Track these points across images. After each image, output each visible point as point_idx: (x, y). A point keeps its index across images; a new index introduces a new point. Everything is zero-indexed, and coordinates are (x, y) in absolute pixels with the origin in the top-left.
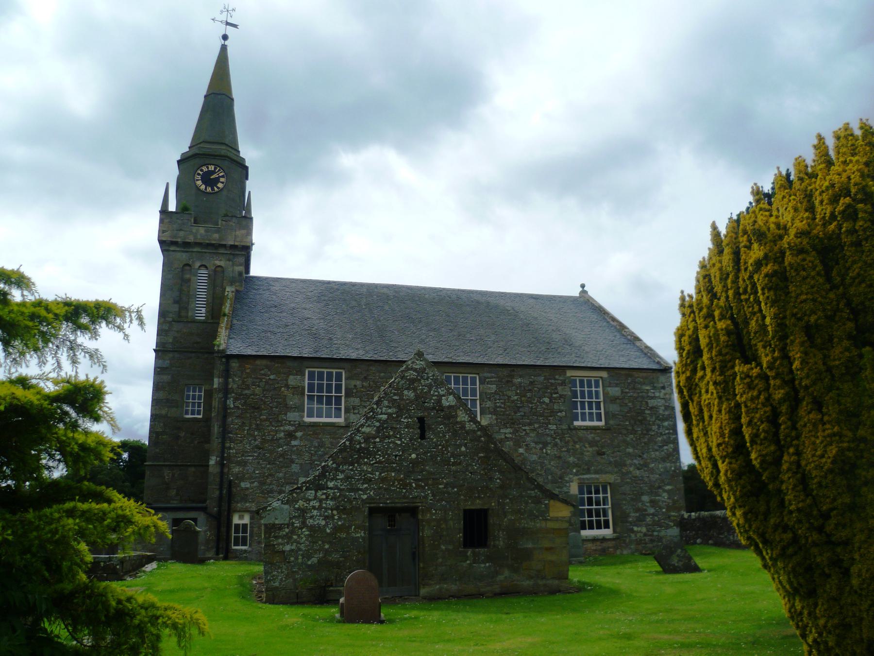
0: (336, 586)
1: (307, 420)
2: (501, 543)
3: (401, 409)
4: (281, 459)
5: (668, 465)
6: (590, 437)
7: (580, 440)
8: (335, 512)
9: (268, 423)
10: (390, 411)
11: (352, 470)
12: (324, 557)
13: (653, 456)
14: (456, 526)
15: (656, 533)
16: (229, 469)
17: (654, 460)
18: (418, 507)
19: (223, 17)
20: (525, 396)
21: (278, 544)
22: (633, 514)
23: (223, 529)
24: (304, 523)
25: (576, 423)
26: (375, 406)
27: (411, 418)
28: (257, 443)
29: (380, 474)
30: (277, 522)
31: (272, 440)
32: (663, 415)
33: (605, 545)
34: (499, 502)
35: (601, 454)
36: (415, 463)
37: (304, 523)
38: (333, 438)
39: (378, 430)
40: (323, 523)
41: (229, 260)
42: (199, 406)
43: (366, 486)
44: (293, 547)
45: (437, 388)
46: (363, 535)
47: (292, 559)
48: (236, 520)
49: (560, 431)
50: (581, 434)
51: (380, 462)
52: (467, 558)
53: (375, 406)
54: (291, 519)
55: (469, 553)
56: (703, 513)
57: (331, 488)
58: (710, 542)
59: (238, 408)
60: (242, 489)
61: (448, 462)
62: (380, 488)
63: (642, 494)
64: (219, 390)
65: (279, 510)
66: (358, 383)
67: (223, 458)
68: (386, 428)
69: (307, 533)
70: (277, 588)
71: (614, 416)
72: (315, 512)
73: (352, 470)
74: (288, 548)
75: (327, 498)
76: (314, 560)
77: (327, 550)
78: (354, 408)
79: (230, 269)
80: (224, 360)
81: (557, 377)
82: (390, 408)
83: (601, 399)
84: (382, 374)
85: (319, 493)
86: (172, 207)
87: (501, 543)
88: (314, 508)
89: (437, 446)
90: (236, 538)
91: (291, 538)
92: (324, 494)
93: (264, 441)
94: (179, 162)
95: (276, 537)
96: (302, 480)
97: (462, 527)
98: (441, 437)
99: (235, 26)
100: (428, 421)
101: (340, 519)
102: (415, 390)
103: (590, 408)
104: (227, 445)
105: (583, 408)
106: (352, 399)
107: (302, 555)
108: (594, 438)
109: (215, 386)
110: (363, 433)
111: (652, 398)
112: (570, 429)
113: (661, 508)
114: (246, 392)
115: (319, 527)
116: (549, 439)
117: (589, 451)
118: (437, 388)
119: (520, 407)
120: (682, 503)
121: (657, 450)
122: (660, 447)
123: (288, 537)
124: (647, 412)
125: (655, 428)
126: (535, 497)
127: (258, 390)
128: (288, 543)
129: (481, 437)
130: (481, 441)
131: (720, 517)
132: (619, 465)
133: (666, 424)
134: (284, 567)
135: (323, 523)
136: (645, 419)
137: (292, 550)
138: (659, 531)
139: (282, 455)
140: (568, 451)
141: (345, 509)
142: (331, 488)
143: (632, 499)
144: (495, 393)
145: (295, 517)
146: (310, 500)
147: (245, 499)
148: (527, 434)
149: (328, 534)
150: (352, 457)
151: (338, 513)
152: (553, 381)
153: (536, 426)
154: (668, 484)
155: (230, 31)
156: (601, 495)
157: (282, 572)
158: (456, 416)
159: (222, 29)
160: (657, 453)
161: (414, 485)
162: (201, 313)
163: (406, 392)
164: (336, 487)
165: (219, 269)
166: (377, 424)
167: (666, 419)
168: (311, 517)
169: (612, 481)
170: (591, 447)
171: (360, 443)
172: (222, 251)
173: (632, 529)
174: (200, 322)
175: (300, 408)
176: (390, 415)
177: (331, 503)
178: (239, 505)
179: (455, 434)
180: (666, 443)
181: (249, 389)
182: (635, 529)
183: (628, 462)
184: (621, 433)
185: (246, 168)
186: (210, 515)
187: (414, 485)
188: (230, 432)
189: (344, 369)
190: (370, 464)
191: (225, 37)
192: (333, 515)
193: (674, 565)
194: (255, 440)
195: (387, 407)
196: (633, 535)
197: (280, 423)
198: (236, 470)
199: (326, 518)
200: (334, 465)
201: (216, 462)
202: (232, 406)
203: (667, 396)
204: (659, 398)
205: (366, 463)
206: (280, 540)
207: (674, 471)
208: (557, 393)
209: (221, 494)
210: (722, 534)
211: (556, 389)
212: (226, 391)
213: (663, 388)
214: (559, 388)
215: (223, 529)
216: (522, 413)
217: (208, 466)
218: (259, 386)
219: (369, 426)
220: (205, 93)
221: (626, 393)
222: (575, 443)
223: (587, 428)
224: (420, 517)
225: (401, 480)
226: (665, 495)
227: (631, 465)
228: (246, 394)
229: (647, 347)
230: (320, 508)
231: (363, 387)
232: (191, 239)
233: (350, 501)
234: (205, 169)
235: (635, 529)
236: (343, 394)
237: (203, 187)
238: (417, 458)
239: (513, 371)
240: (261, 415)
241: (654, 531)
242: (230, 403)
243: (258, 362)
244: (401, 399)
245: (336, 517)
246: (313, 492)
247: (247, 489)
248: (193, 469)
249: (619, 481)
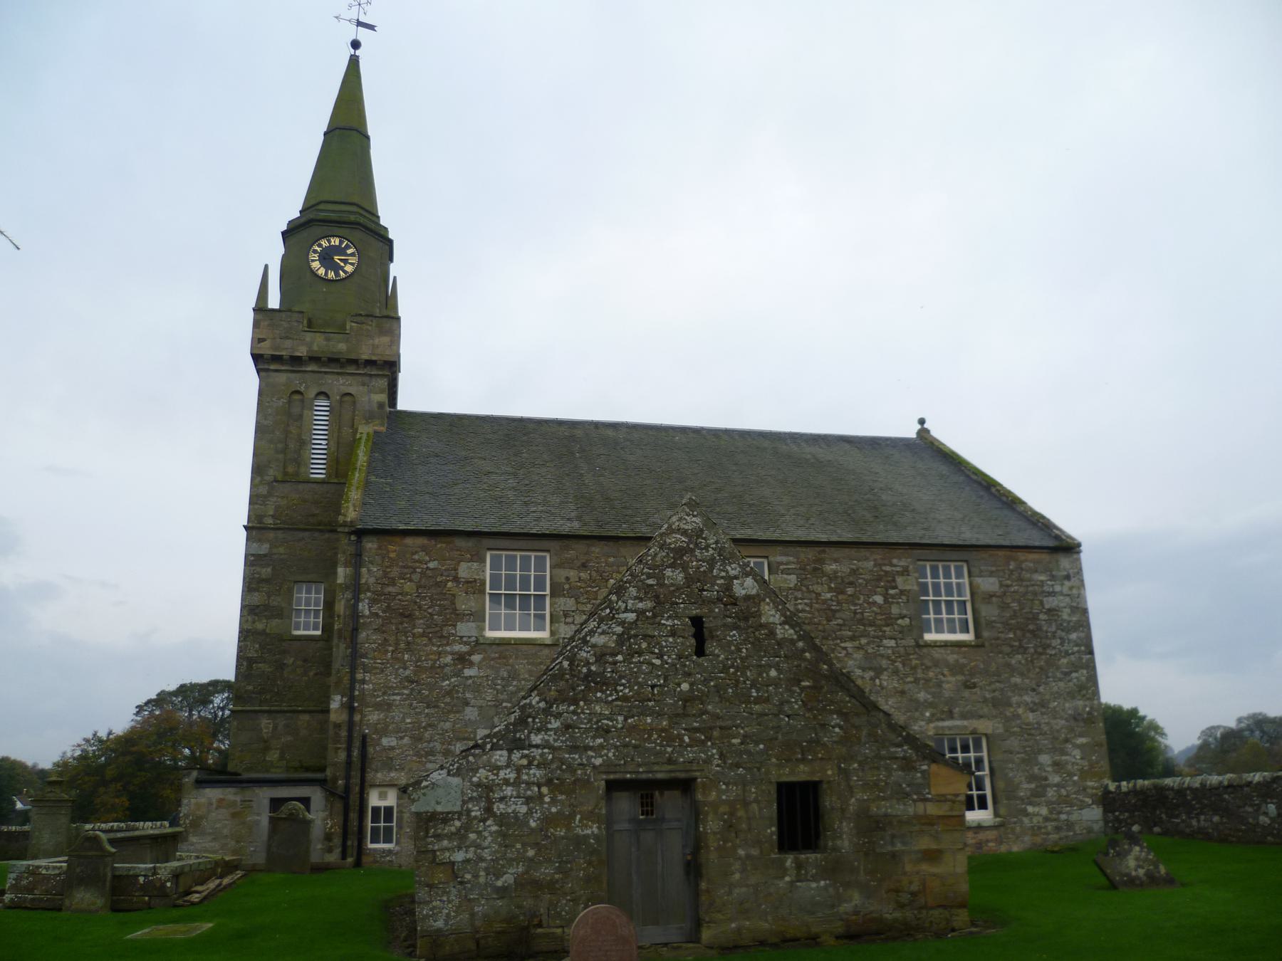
0: (549, 927)
1: (490, 634)
2: (845, 844)
3: (661, 600)
4: (448, 700)
5: (1081, 703)
6: (952, 658)
7: (936, 664)
8: (545, 790)
9: (425, 641)
10: (640, 605)
11: (574, 712)
12: (527, 872)
13: (1055, 689)
14: (763, 818)
15: (1063, 817)
16: (363, 716)
17: (1057, 696)
18: (695, 779)
19: (353, 14)
20: (843, 593)
21: (443, 850)
22: (1026, 786)
23: (353, 816)
24: (489, 810)
25: (928, 637)
26: (614, 598)
27: (677, 617)
28: (407, 672)
29: (626, 719)
30: (439, 809)
31: (432, 667)
32: (1069, 622)
33: (982, 836)
34: (839, 767)
35: (969, 686)
36: (688, 699)
37: (489, 810)
38: (532, 664)
39: (621, 639)
40: (524, 809)
41: (363, 385)
42: (316, 616)
43: (600, 741)
44: (470, 855)
45: (724, 564)
46: (596, 831)
47: (468, 876)
48: (374, 800)
49: (902, 650)
50: (937, 654)
51: (625, 699)
52: (784, 871)
53: (614, 598)
54: (464, 802)
55: (788, 863)
56: (1140, 782)
57: (537, 746)
58: (1157, 829)
59: (377, 615)
60: (384, 749)
61: (747, 699)
62: (626, 745)
63: (1040, 752)
64: (346, 587)
65: (446, 790)
66: (572, 574)
67: (352, 698)
68: (636, 636)
69: (494, 828)
70: (439, 930)
71: (990, 624)
72: (509, 791)
73: (574, 712)
74: (459, 856)
75: (530, 764)
76: (508, 879)
77: (531, 860)
78: (566, 616)
79: (365, 399)
80: (353, 538)
81: (895, 561)
82: (641, 600)
83: (968, 597)
84: (612, 559)
85: (516, 755)
86: (274, 302)
87: (846, 843)
88: (506, 782)
89: (725, 669)
90: (375, 831)
91: (464, 837)
92: (523, 756)
93: (419, 669)
94: (283, 233)
95: (439, 837)
96: (482, 732)
97: (775, 815)
98: (732, 653)
99: (371, 27)
100: (708, 623)
101: (554, 801)
102: (685, 568)
103: (950, 611)
104: (359, 676)
105: (938, 611)
106: (562, 600)
107: (486, 869)
108: (957, 661)
109: (340, 580)
110: (594, 646)
111: (1053, 594)
112: (918, 646)
113: (1071, 775)
114: (390, 589)
115: (516, 818)
116: (884, 663)
117: (950, 683)
118: (724, 564)
119: (835, 611)
120: (1105, 765)
121: (1060, 680)
122: (1066, 674)
123: (460, 836)
124: (1042, 617)
125: (1056, 642)
126: (904, 758)
127: (409, 587)
128: (460, 848)
129: (803, 651)
130: (805, 660)
131: (1172, 789)
132: (999, 704)
133: (1074, 636)
134: (454, 891)
135: (524, 809)
136: (1039, 628)
137: (467, 861)
138: (1068, 813)
139: (449, 693)
140: (916, 681)
141: (562, 781)
142: (537, 746)
143: (1023, 761)
144: (796, 588)
145: (471, 799)
146: (499, 768)
147: (388, 765)
148: (848, 655)
149: (532, 830)
150: (574, 689)
151: (551, 791)
152: (888, 568)
153: (864, 641)
154: (1081, 735)
155: (363, 34)
156: (972, 755)
157: (449, 902)
158: (758, 614)
159: (352, 32)
160: (1061, 684)
161: (686, 739)
162: (318, 470)
163: (668, 572)
164: (546, 745)
165: (347, 398)
166: (619, 629)
167: (1075, 629)
168: (502, 799)
169: (989, 732)
170: (953, 675)
171: (588, 664)
172: (351, 369)
173: (1025, 810)
174: (316, 482)
175: (478, 616)
176: (641, 613)
177: (536, 773)
178: (379, 775)
179: (757, 644)
180: (1075, 667)
181: (394, 585)
182: (1030, 809)
183: (1015, 699)
184: (1001, 652)
185: (390, 242)
186: (331, 793)
187: (686, 739)
188: (365, 656)
189: (548, 551)
190: (607, 702)
191: (356, 45)
192: (541, 796)
193: (1128, 875)
194: (405, 669)
195: (636, 598)
196: (1026, 820)
197: (446, 639)
198: (374, 717)
199: (528, 800)
200: (542, 705)
201: (342, 704)
202: (367, 612)
203: (1075, 591)
204: (1061, 593)
205: (599, 700)
206: (445, 843)
207: (1089, 713)
208: (895, 587)
209: (349, 756)
210: (1177, 817)
211: (894, 580)
212: (356, 588)
213: (1068, 577)
214: (899, 580)
215: (353, 816)
216: (840, 621)
217: (327, 711)
218: (411, 580)
219: (603, 633)
220: (324, 127)
221: (1008, 586)
222: (928, 668)
223: (945, 645)
224: (699, 797)
225: (663, 730)
226: (1077, 754)
227: (1019, 705)
228: (389, 593)
229: (1035, 514)
230: (517, 783)
231: (580, 580)
232: (302, 351)
233: (571, 769)
234: (324, 243)
235: (1030, 809)
236: (548, 592)
237: (322, 272)
238: (691, 690)
239: (824, 552)
240: (414, 627)
241: (1060, 813)
242: (364, 607)
243: (409, 541)
244: (661, 585)
245: (547, 799)
246: (505, 753)
247: (392, 748)
248: (306, 717)
249: (1001, 730)
